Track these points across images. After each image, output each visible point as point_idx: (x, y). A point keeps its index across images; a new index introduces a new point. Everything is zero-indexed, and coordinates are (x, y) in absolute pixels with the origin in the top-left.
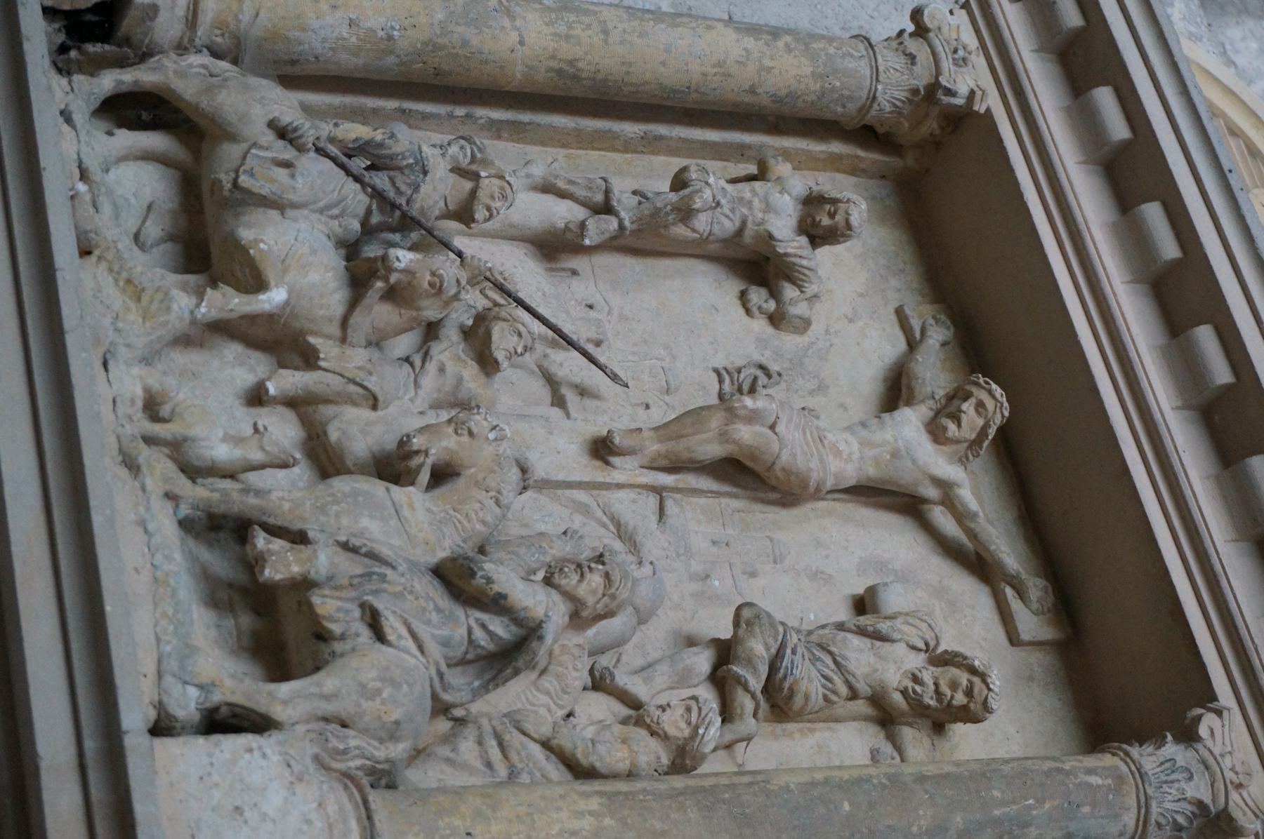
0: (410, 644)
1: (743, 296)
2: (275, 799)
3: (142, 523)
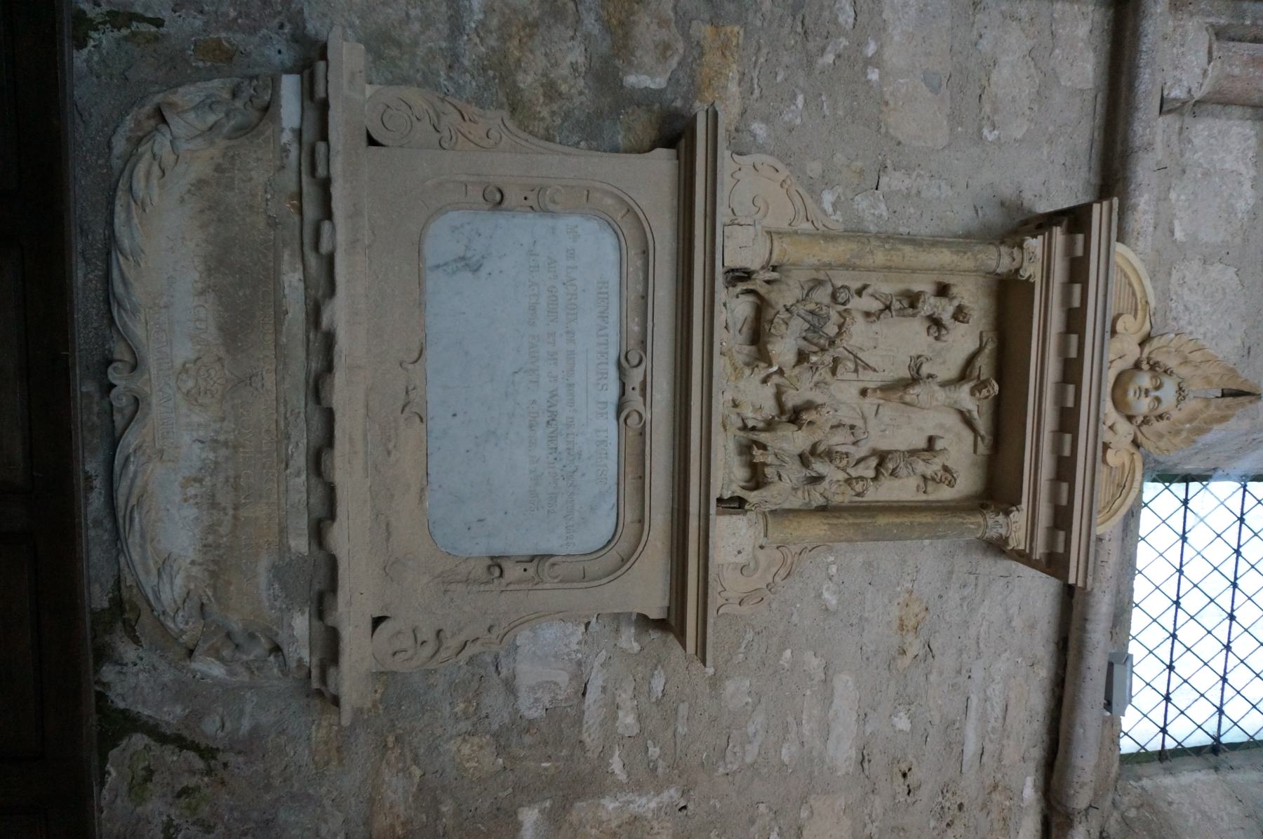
0: (788, 481)
1: (929, 328)
2: (744, 531)
3: (725, 446)
